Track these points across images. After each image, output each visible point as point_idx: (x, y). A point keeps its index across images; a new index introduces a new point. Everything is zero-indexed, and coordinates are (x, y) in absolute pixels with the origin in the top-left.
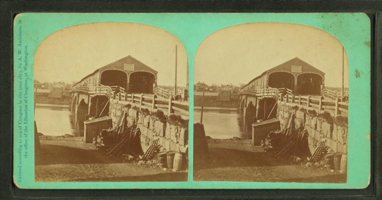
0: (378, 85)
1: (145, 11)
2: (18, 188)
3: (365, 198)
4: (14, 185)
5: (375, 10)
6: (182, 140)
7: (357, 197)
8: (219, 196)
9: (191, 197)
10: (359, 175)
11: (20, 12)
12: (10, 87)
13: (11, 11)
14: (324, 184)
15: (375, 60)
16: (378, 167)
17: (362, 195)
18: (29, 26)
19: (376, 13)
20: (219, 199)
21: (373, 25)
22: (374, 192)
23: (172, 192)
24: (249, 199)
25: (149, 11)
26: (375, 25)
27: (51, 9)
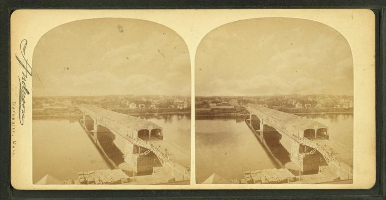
0: (383, 44)
1: (145, 7)
2: (15, 189)
3: (371, 198)
4: (11, 187)
5: (381, 5)
6: (23, 90)
7: (362, 198)
8: (222, 197)
9: (193, 197)
10: (364, 176)
11: (18, 8)
12: (8, 86)
13: (8, 8)
14: (336, 185)
15: (381, 56)
16: (384, 167)
17: (367, 196)
18: (29, 28)
19: (382, 8)
20: (364, 199)
21: (378, 27)
22: (381, 192)
23: (173, 193)
24: (253, 199)
25: (150, 7)
26: (381, 22)
27: (50, 6)
